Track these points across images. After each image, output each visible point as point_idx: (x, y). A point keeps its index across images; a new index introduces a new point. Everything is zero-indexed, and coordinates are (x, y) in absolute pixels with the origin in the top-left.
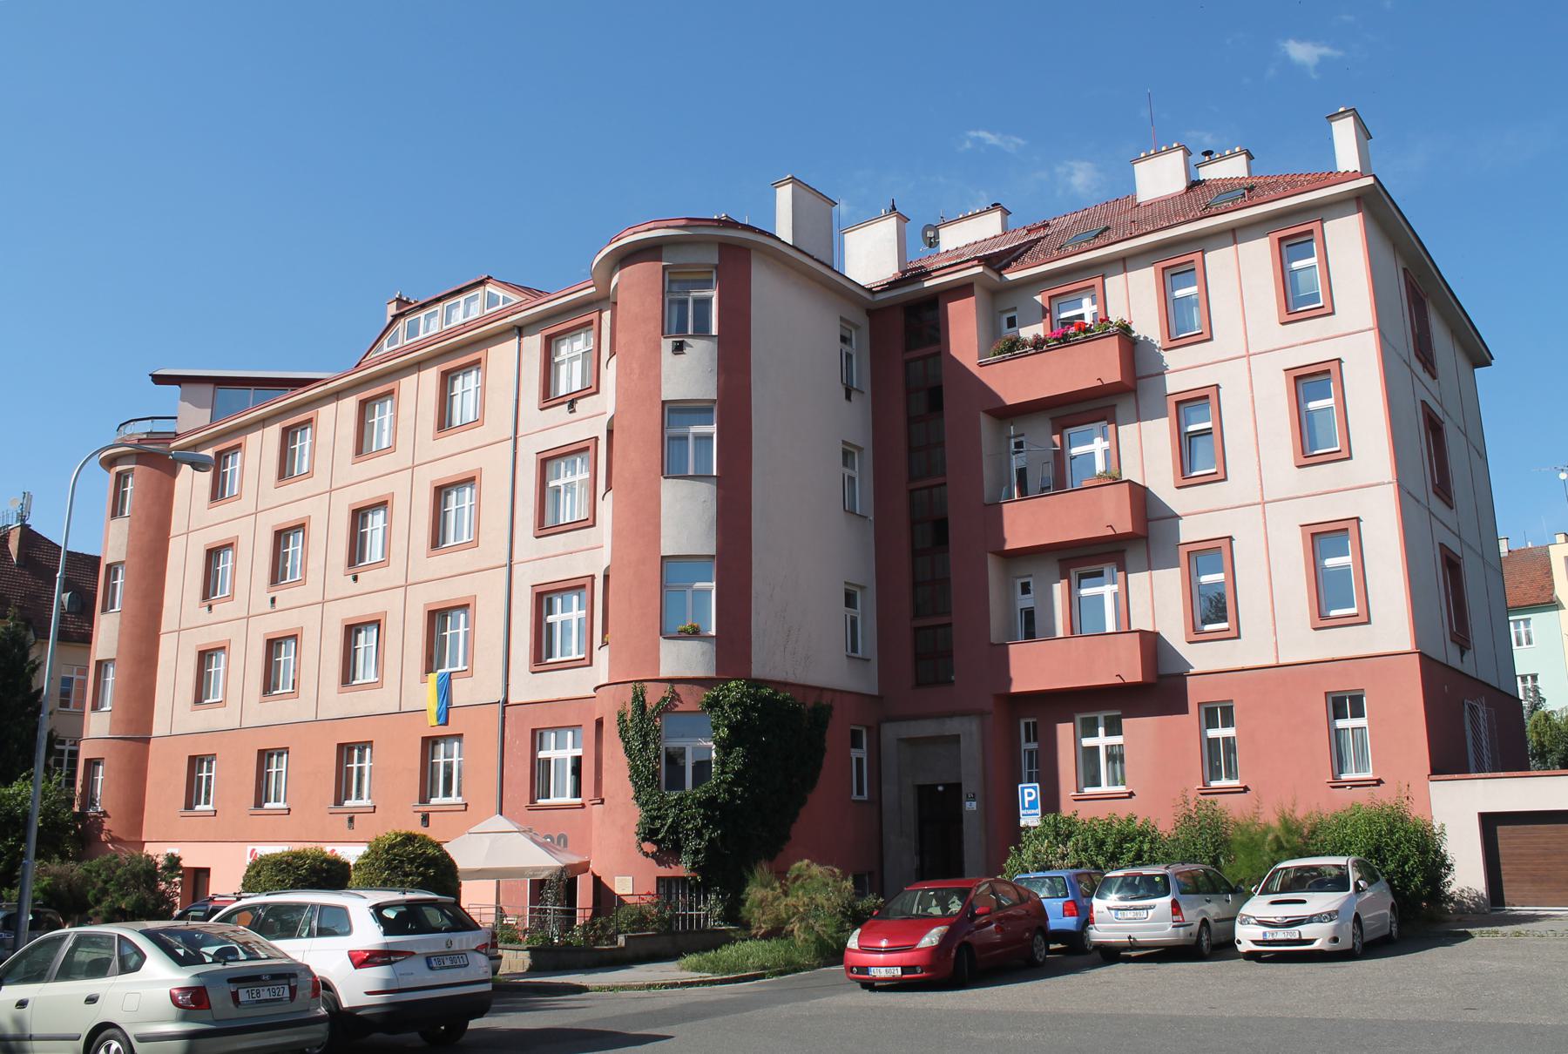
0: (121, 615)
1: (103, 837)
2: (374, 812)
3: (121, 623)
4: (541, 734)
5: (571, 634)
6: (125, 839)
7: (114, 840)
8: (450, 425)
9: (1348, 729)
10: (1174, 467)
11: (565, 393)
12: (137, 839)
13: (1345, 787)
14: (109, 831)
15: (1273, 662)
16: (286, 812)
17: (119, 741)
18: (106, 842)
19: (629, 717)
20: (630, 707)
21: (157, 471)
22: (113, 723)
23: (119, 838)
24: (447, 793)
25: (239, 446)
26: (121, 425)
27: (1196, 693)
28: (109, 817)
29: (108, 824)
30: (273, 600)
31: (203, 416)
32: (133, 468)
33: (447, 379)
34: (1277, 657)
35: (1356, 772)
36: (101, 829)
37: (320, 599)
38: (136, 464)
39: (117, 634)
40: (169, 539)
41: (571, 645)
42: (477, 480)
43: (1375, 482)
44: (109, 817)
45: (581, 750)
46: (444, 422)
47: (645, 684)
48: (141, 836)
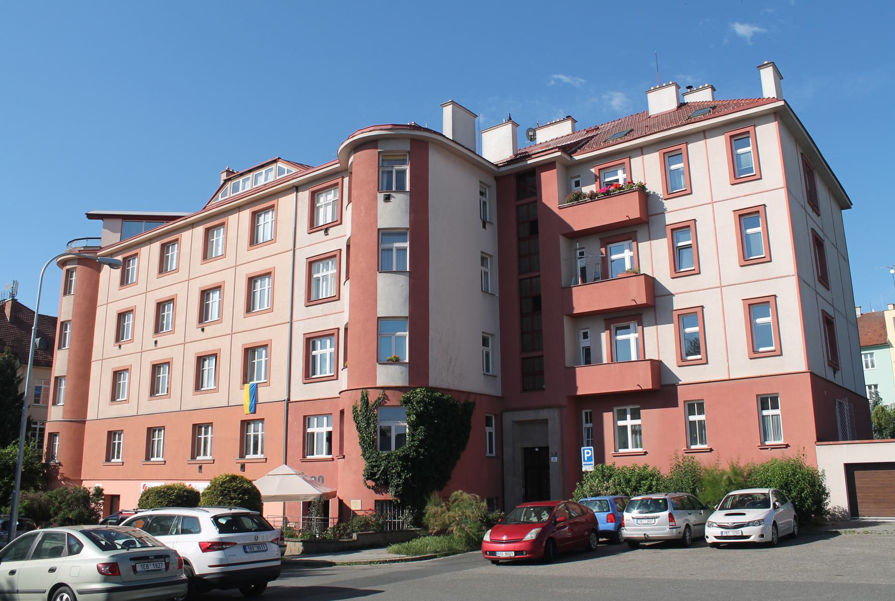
0: (69, 351)
1: (59, 477)
2: (214, 463)
3: (69, 355)
4: (309, 419)
5: (326, 362)
6: (71, 478)
7: (65, 479)
8: (257, 242)
9: (769, 416)
10: (670, 266)
11: (322, 224)
12: (78, 478)
13: (768, 449)
14: (62, 474)
15: (727, 378)
16: (164, 463)
17: (68, 422)
18: (61, 480)
19: (359, 409)
20: (359, 403)
21: (90, 269)
22: (65, 412)
23: (68, 478)
24: (255, 452)
25: (136, 254)
26: (69, 242)
27: (683, 395)
28: (62, 466)
29: (61, 470)
30: (156, 342)
31: (116, 237)
32: (76, 267)
33: (255, 216)
34: (729, 375)
35: (774, 440)
36: (57, 473)
37: (183, 342)
38: (78, 264)
39: (66, 362)
40: (96, 308)
41: (326, 368)
42: (272, 274)
43: (785, 275)
44: (62, 466)
45: (332, 428)
46: (253, 241)
47: (368, 390)
48: (80, 477)
